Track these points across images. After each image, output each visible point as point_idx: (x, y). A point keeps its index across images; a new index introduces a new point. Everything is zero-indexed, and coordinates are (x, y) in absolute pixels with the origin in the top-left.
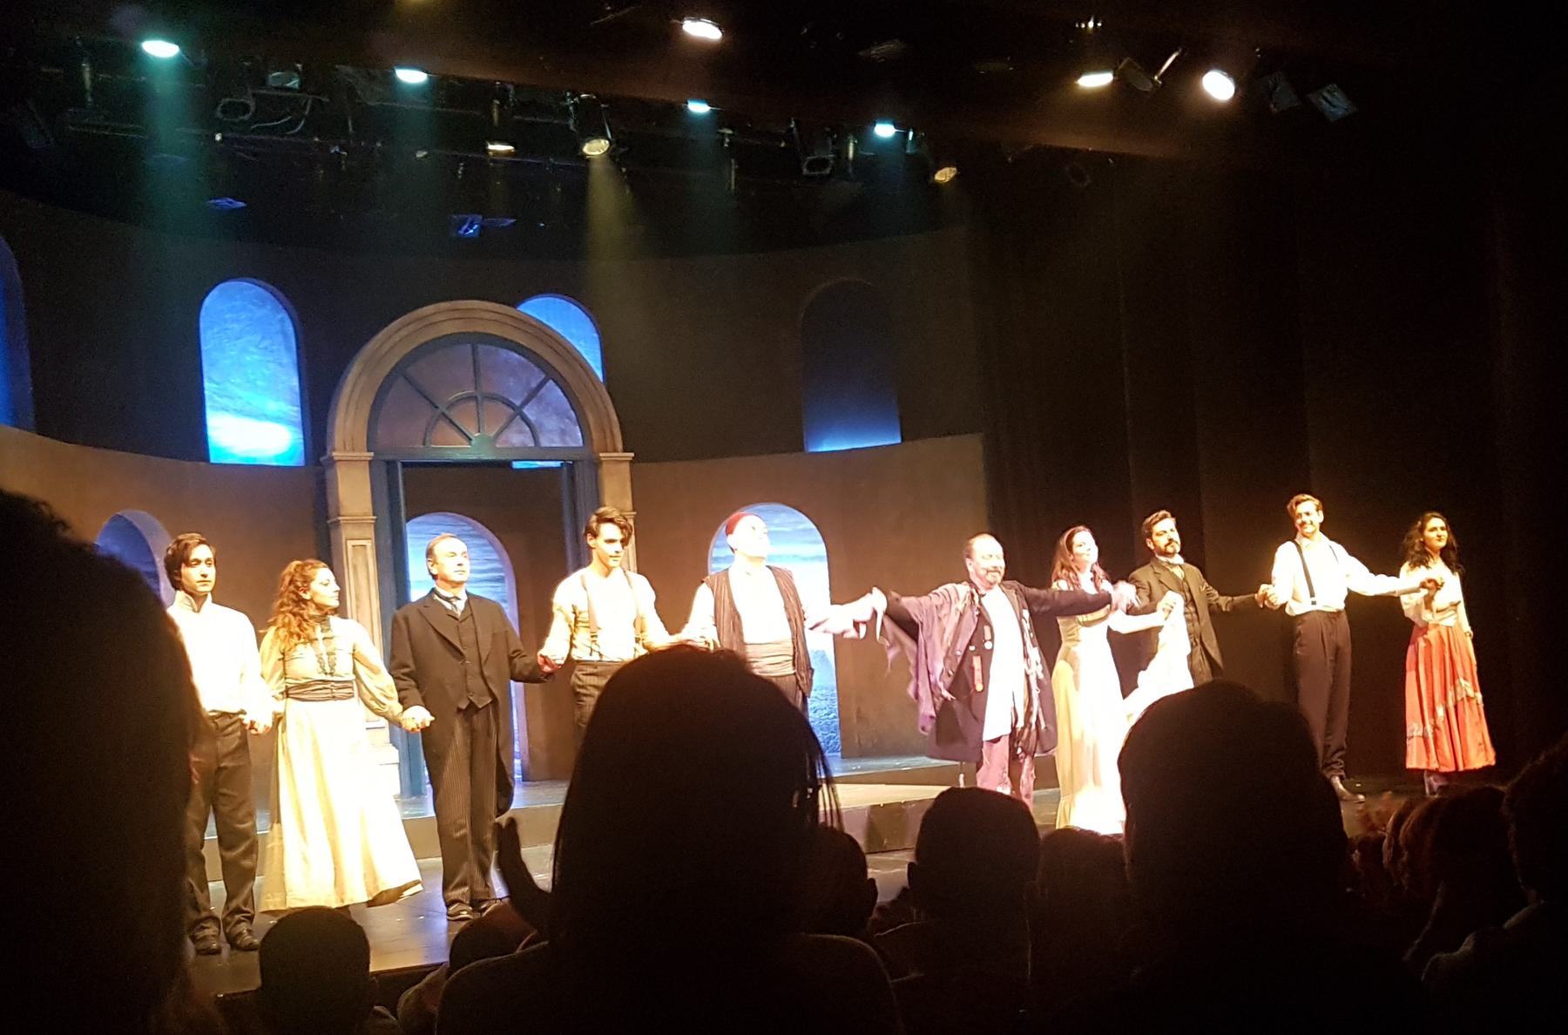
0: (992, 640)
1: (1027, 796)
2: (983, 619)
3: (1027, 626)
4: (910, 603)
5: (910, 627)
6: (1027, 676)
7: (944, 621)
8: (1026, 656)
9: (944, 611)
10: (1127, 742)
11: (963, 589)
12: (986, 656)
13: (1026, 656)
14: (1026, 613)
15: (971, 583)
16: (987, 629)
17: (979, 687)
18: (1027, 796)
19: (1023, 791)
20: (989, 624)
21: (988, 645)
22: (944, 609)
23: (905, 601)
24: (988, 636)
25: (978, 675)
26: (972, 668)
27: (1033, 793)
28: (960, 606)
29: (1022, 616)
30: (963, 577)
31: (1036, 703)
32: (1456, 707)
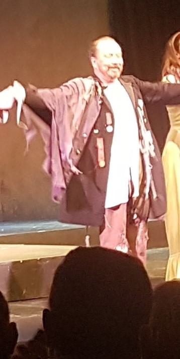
0: (113, 125)
1: (142, 254)
2: (105, 107)
3: (141, 113)
4: (45, 94)
5: (44, 114)
6: (142, 155)
7: (73, 109)
8: (141, 138)
9: (73, 101)
11: (89, 82)
12: (108, 139)
13: (141, 138)
14: (141, 103)
15: (95, 77)
16: (108, 115)
17: (102, 164)
21: (109, 129)
22: (72, 98)
23: (41, 92)
24: (109, 121)
25: (101, 153)
26: (96, 148)
27: (147, 252)
28: (87, 97)
30: (89, 72)
31: (101, 153)
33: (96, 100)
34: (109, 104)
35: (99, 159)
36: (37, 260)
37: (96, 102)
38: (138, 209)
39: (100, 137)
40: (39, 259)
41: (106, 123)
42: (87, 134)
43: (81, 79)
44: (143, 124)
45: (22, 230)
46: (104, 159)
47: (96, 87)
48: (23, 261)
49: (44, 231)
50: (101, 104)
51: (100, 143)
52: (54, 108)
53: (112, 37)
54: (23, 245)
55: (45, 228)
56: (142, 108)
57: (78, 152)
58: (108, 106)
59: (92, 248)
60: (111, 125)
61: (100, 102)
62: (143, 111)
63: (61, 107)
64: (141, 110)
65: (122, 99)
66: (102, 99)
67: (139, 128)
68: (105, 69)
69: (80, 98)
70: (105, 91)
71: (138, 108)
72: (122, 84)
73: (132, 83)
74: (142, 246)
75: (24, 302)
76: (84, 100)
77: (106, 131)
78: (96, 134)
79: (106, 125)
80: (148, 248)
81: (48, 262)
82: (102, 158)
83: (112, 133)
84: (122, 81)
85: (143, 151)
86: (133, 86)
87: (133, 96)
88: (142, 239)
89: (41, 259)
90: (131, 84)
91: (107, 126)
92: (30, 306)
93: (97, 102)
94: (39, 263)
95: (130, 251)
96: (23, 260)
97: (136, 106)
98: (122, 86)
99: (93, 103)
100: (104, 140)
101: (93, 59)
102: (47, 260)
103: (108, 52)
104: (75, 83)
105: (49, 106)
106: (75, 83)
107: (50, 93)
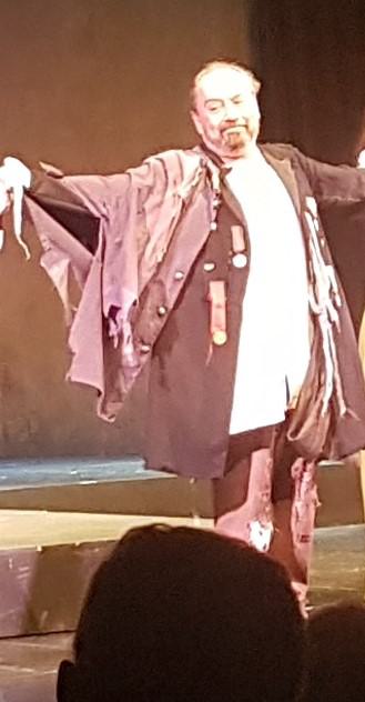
0: (246, 252)
1: (304, 539)
2: (227, 213)
3: (314, 226)
4: (88, 188)
5: (84, 226)
6: (314, 317)
7: (149, 219)
8: (312, 279)
9: (154, 199)
10: (234, 370)
11: (192, 161)
12: (235, 282)
13: (312, 279)
14: (311, 203)
15: (204, 147)
16: (236, 230)
17: (220, 338)
18: (304, 539)
19: (297, 529)
20: (241, 223)
21: (239, 261)
22: (152, 200)
23: (67, 181)
24: (239, 245)
25: (219, 315)
26: (207, 302)
27: (314, 533)
28: (183, 191)
29: (304, 208)
30: (189, 139)
31: (219, 315)
32: (62, 481)
33: (207, 197)
34: (238, 206)
35: (214, 329)
36: (73, 547)
37: (206, 203)
38: (131, 378)
39: (219, 279)
40: (77, 543)
41: (232, 249)
42: (183, 273)
43: (180, 152)
44: (318, 250)
45: (46, 478)
46: (224, 327)
47: (209, 174)
48: (43, 548)
49: (95, 482)
50: (217, 209)
51: (217, 292)
52: (104, 211)
53: (229, 60)
54: (45, 512)
55: (95, 476)
56: (316, 215)
57: (162, 310)
58: (235, 210)
59: (267, 558)
60: (242, 253)
61: (216, 203)
62: (316, 222)
63: (123, 211)
64: (313, 219)
65: (267, 195)
66: (220, 196)
67: (308, 257)
68: (215, 135)
69: (169, 193)
70: (229, 178)
71: (307, 215)
72: (269, 163)
73: (292, 161)
74: (305, 520)
75: (44, 638)
76: (179, 197)
77: (231, 267)
78: (209, 272)
79: (231, 253)
80: (317, 525)
81: (97, 550)
82: (219, 326)
83: (247, 268)
84: (268, 156)
85: (316, 309)
86: (293, 167)
87: (296, 191)
88: (307, 506)
89: (81, 545)
90: (289, 163)
91: (234, 254)
92: (55, 647)
93: (209, 203)
94: (77, 553)
95: (277, 530)
96: (45, 545)
97: (302, 210)
98: (269, 167)
99: (199, 198)
100: (227, 286)
101: (195, 118)
102: (93, 548)
103: (227, 92)
104: (161, 160)
105: (92, 209)
106: (161, 160)
107: (101, 183)
